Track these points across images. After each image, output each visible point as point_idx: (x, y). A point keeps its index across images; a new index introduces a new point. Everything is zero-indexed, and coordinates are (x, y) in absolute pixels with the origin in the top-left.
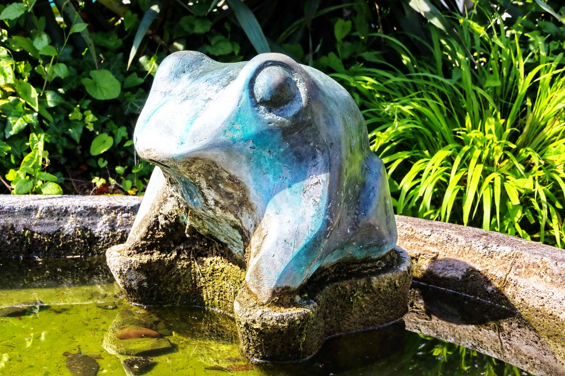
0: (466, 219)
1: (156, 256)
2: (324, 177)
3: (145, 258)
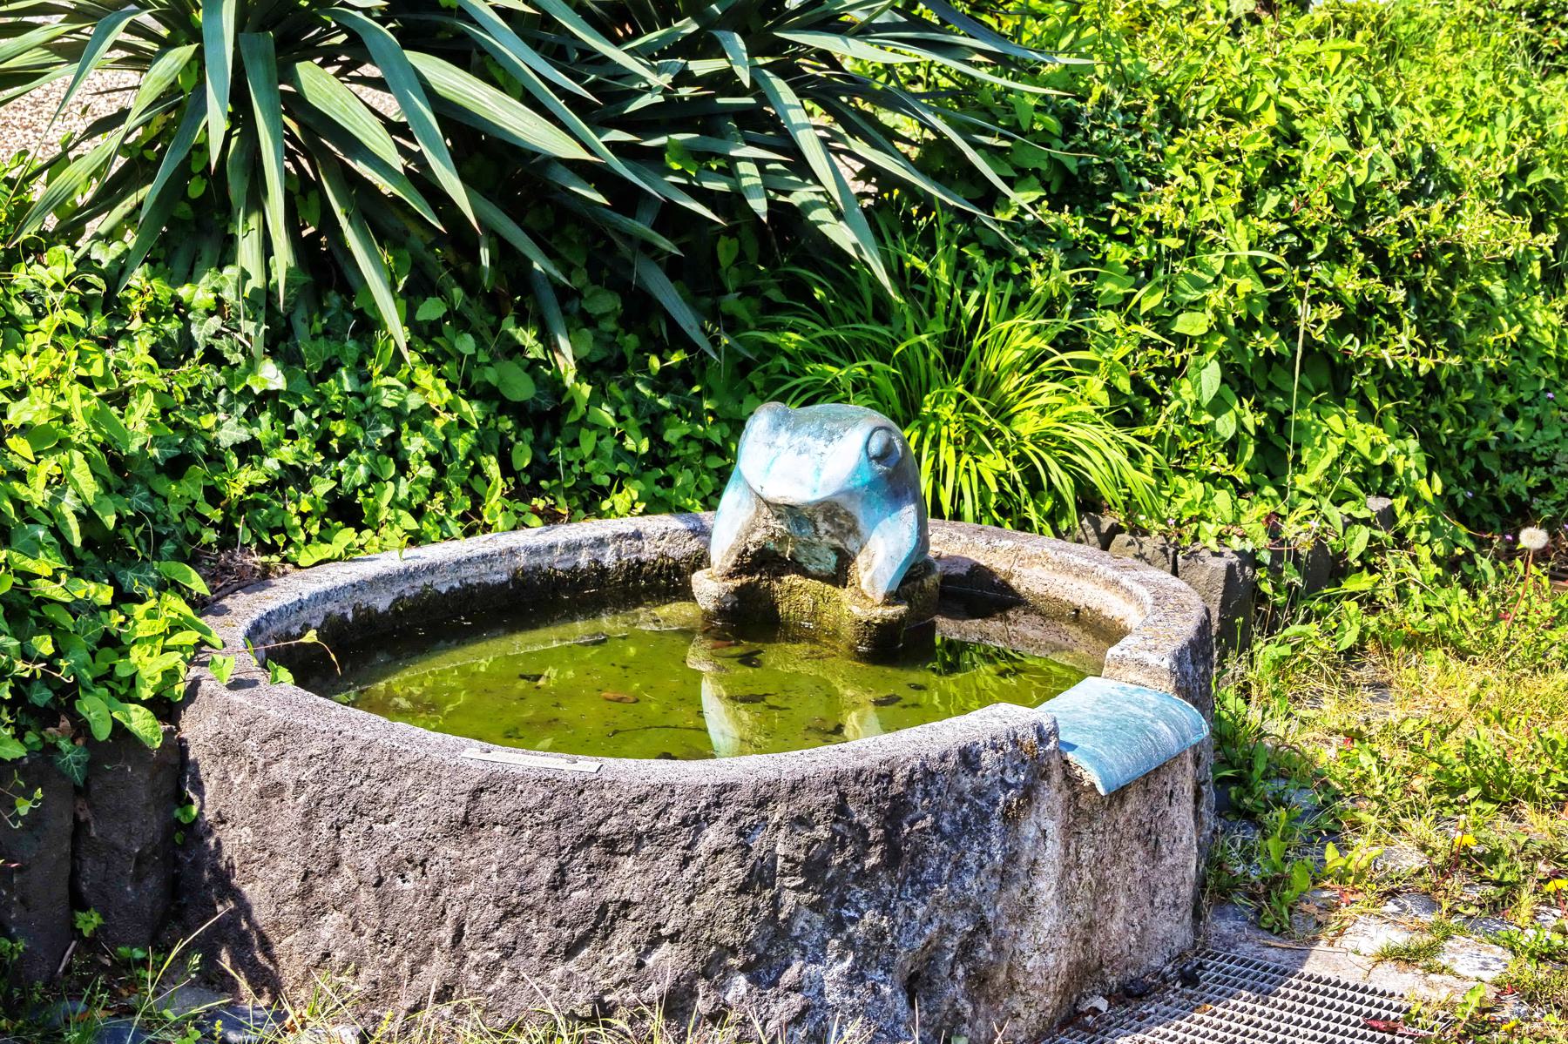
0: (946, 513)
1: (745, 580)
2: (913, 507)
3: (738, 583)
